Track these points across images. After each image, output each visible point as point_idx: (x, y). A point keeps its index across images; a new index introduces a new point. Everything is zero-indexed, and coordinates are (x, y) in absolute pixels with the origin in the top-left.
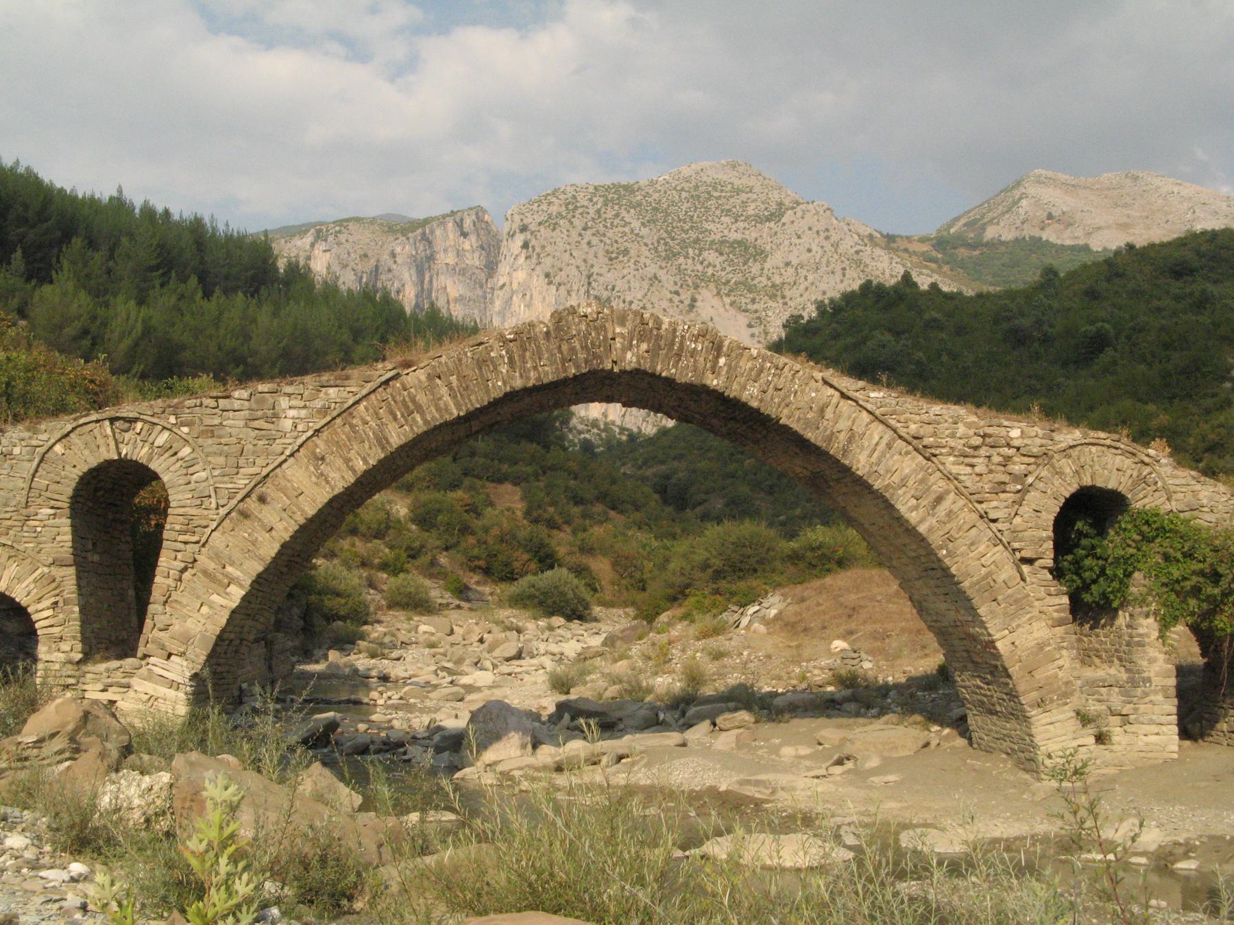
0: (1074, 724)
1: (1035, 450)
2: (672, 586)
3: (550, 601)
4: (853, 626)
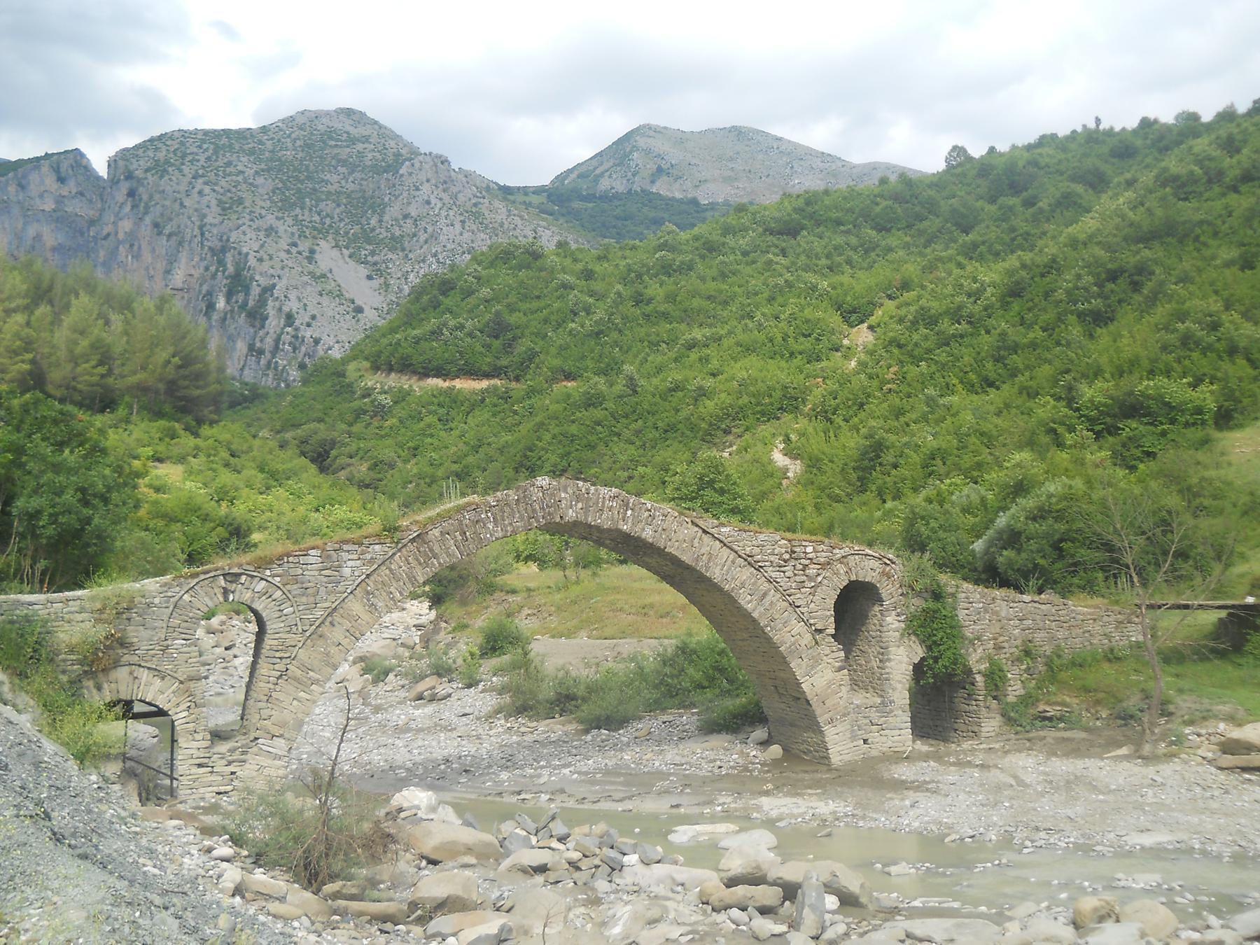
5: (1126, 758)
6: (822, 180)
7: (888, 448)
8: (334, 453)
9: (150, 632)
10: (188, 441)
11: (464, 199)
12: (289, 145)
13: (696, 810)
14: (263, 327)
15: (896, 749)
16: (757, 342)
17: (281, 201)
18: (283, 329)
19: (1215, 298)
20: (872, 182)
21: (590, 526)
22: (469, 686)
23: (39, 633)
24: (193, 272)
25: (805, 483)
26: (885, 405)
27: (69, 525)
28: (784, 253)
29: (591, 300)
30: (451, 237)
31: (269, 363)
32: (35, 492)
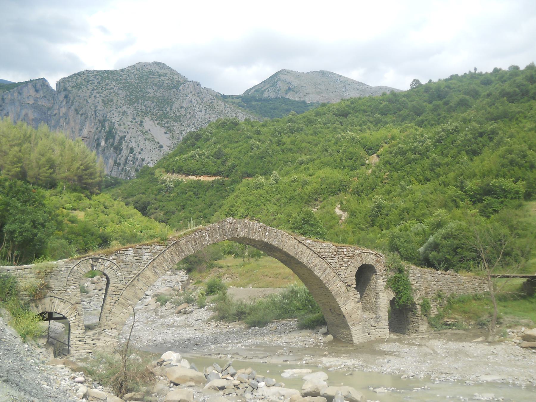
5: (481, 342)
6: (358, 93)
7: (384, 207)
8: (149, 207)
9: (59, 283)
10: (87, 202)
11: (206, 100)
12: (133, 77)
13: (294, 363)
14: (120, 153)
15: (382, 337)
16: (329, 162)
17: (129, 100)
18: (129, 154)
19: (525, 144)
20: (378, 95)
21: (250, 239)
22: (201, 308)
23: (12, 283)
24: (91, 130)
25: (348, 222)
26: (383, 189)
27: (27, 237)
28: (341, 124)
29: (259, 143)
30: (201, 116)
31: (123, 169)
32: (13, 222)
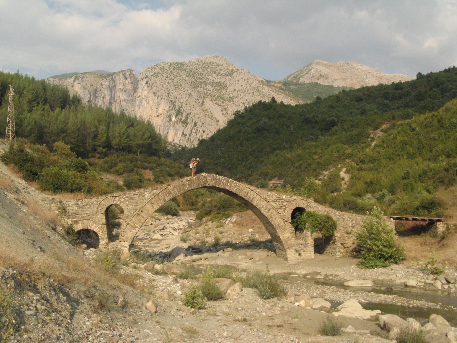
0: (294, 252)
1: (288, 200)
2: (207, 211)
3: (167, 210)
4: (254, 225)
24: (165, 108)
31: (189, 138)
